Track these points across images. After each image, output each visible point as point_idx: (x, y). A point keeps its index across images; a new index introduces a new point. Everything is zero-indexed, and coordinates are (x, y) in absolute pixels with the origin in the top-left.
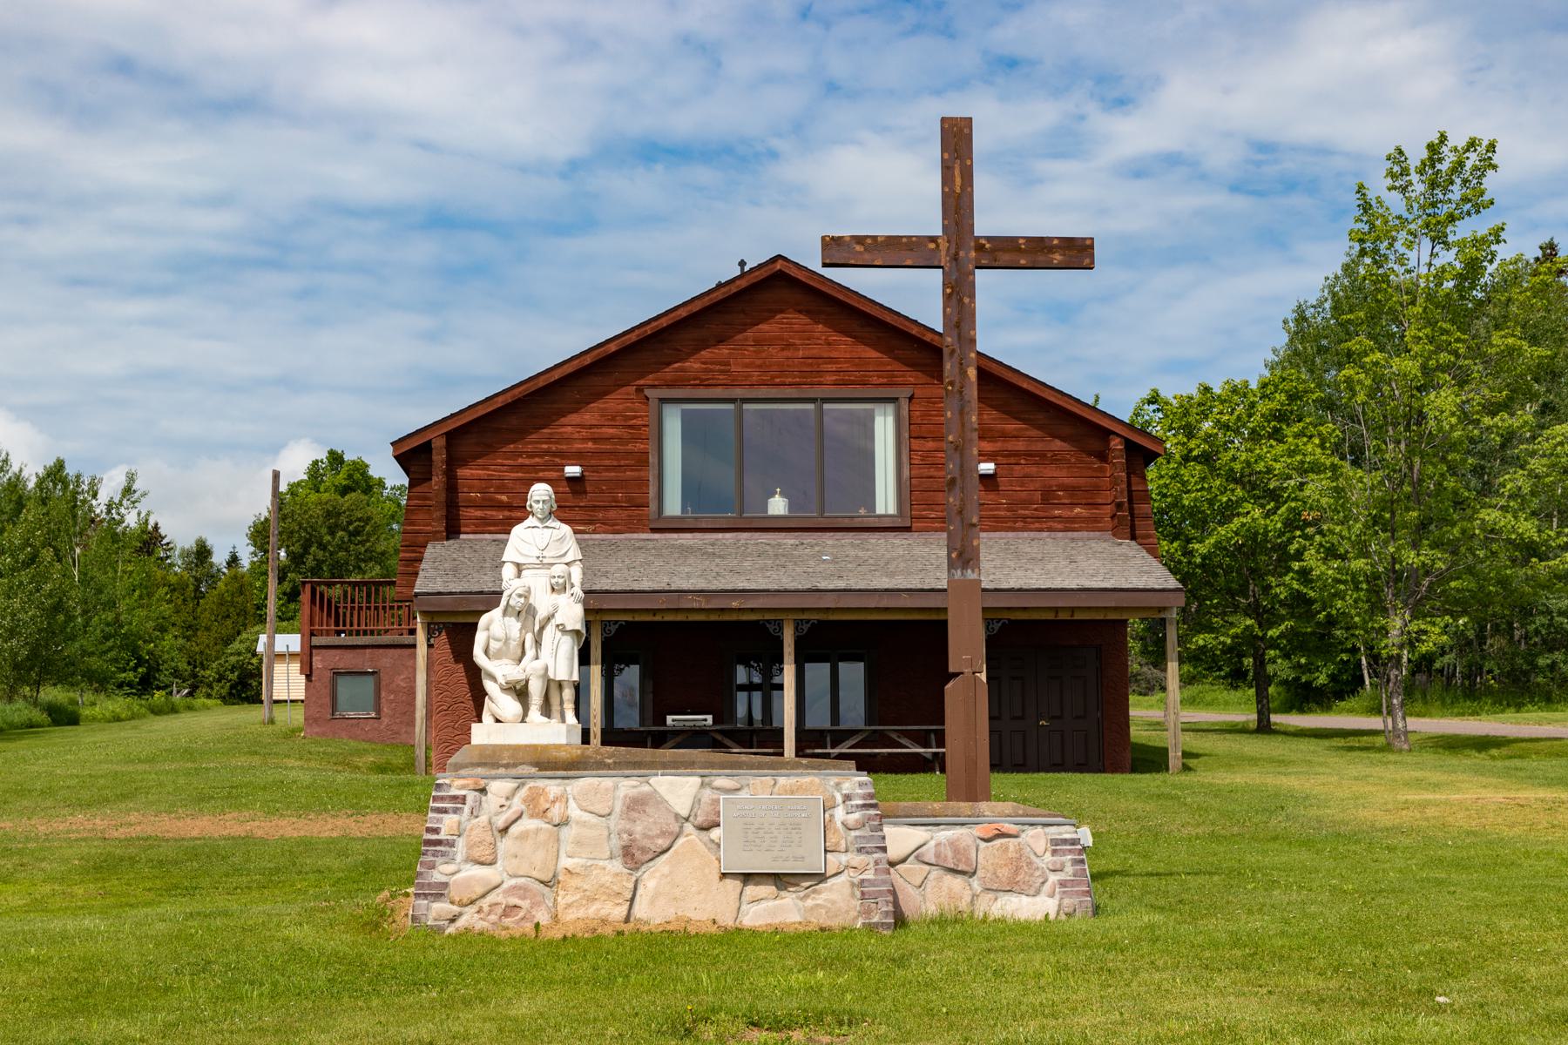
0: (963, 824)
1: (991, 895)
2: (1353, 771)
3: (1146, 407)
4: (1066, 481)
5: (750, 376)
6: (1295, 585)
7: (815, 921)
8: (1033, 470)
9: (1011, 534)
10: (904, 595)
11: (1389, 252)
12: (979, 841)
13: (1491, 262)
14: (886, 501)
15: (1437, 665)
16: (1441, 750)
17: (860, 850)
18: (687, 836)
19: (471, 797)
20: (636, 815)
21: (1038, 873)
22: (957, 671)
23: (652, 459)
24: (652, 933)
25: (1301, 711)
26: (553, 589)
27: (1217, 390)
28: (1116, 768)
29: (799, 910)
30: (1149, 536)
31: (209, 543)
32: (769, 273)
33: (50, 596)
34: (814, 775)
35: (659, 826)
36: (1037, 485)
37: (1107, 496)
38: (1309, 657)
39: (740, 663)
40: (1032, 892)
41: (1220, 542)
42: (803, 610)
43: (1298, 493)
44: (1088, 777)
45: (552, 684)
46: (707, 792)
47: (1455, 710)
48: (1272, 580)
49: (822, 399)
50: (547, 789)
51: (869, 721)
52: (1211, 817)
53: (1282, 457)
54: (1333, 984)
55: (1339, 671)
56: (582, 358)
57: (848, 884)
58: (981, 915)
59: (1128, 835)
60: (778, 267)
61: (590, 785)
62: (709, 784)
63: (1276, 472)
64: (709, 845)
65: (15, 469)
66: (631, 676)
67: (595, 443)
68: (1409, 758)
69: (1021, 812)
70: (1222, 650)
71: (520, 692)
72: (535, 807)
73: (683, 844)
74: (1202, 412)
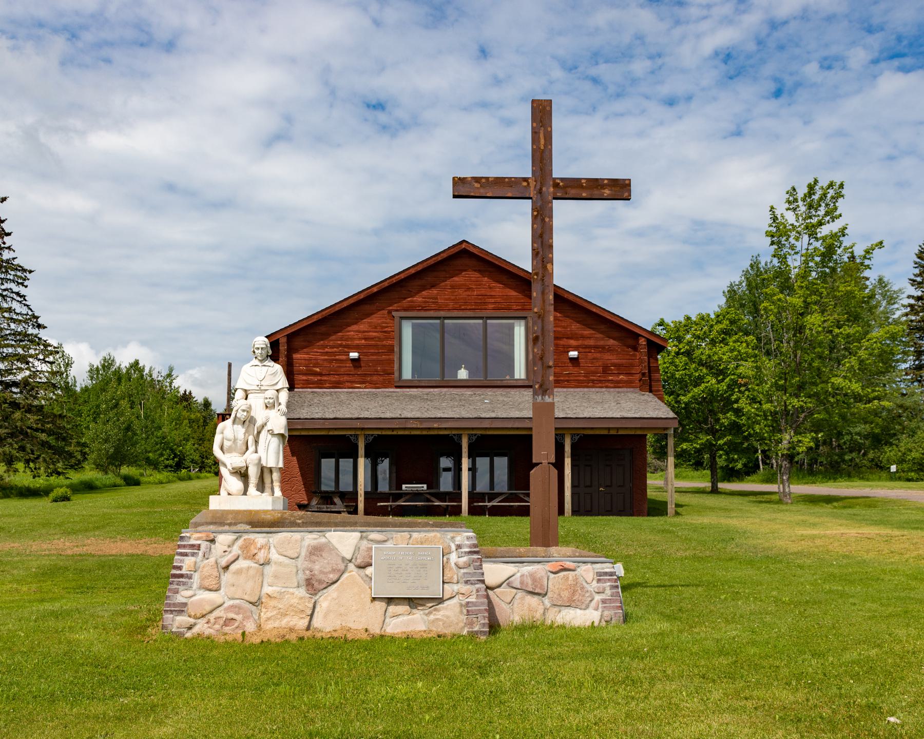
0: (539, 562)
1: (557, 609)
2: (767, 516)
3: (657, 327)
4: (616, 361)
5: (448, 305)
6: (733, 418)
7: (435, 629)
8: (598, 355)
9: (586, 389)
10: (527, 421)
11: (786, 243)
12: (549, 573)
13: (839, 247)
14: (520, 372)
15: (796, 459)
16: (807, 503)
17: (466, 582)
18: (350, 572)
19: (204, 545)
20: (315, 558)
21: (587, 595)
22: (538, 462)
23: (396, 349)
24: (322, 638)
25: (729, 481)
26: (267, 407)
27: (694, 319)
28: (639, 513)
29: (425, 622)
30: (659, 391)
31: (210, 400)
32: (459, 250)
33: (124, 423)
34: (437, 531)
35: (330, 566)
36: (600, 363)
37: (637, 370)
38: (738, 454)
39: (442, 456)
40: (583, 607)
41: (694, 396)
42: (473, 429)
43: (735, 371)
44: (624, 519)
45: (265, 470)
46: (365, 542)
47: (804, 481)
48: (721, 416)
49: (486, 317)
50: (256, 541)
51: (510, 489)
52: (693, 545)
53: (727, 352)
54: (800, 696)
55: (748, 462)
56: (359, 295)
57: (458, 605)
58: (550, 621)
59: (646, 556)
60: (464, 247)
61: (285, 537)
62: (366, 538)
63: (724, 360)
64: (365, 579)
65: (118, 365)
66: (384, 466)
67: (365, 341)
68: (793, 508)
69: (577, 554)
70: (694, 451)
71: (243, 474)
72: (247, 552)
73: (347, 578)
74: (686, 330)
